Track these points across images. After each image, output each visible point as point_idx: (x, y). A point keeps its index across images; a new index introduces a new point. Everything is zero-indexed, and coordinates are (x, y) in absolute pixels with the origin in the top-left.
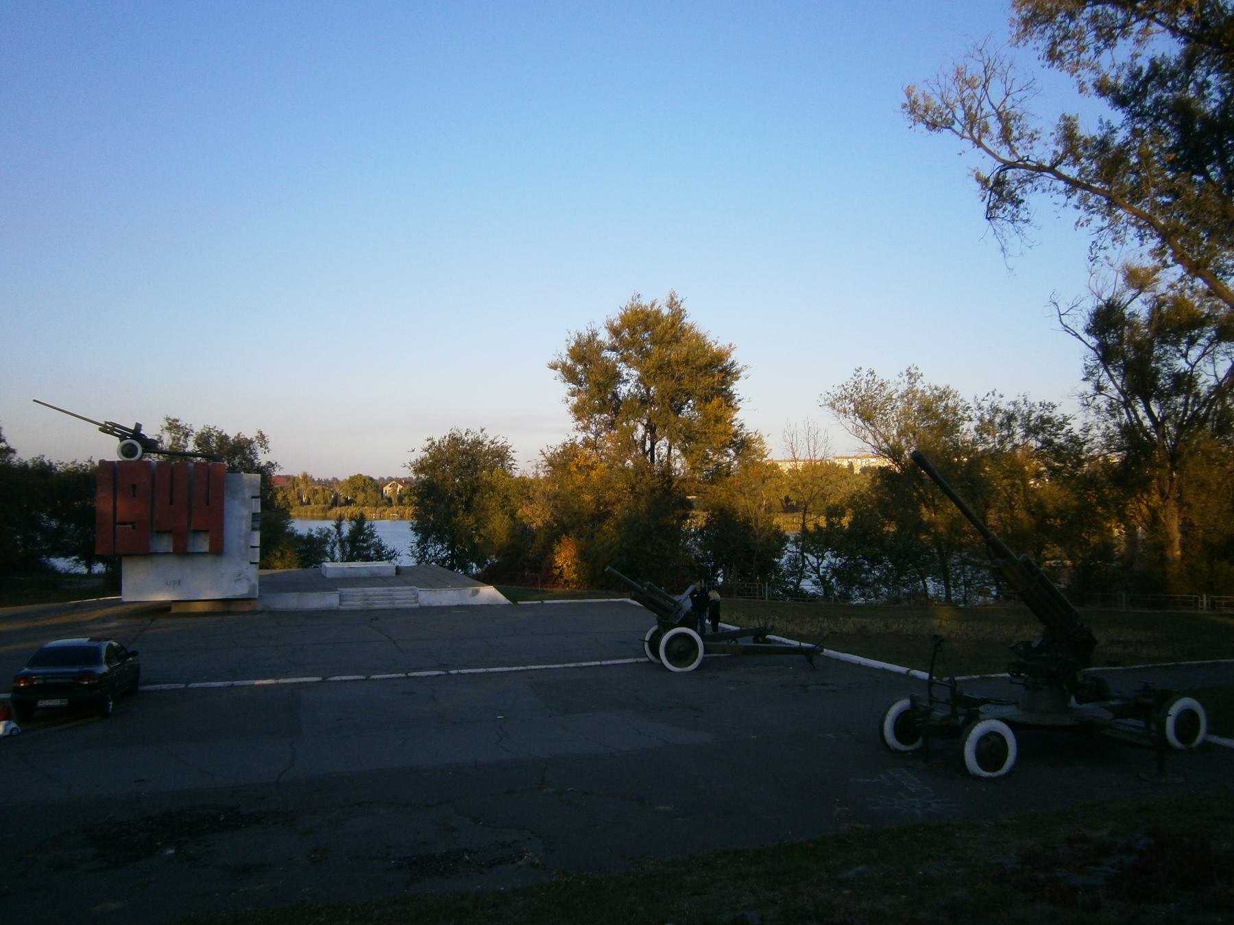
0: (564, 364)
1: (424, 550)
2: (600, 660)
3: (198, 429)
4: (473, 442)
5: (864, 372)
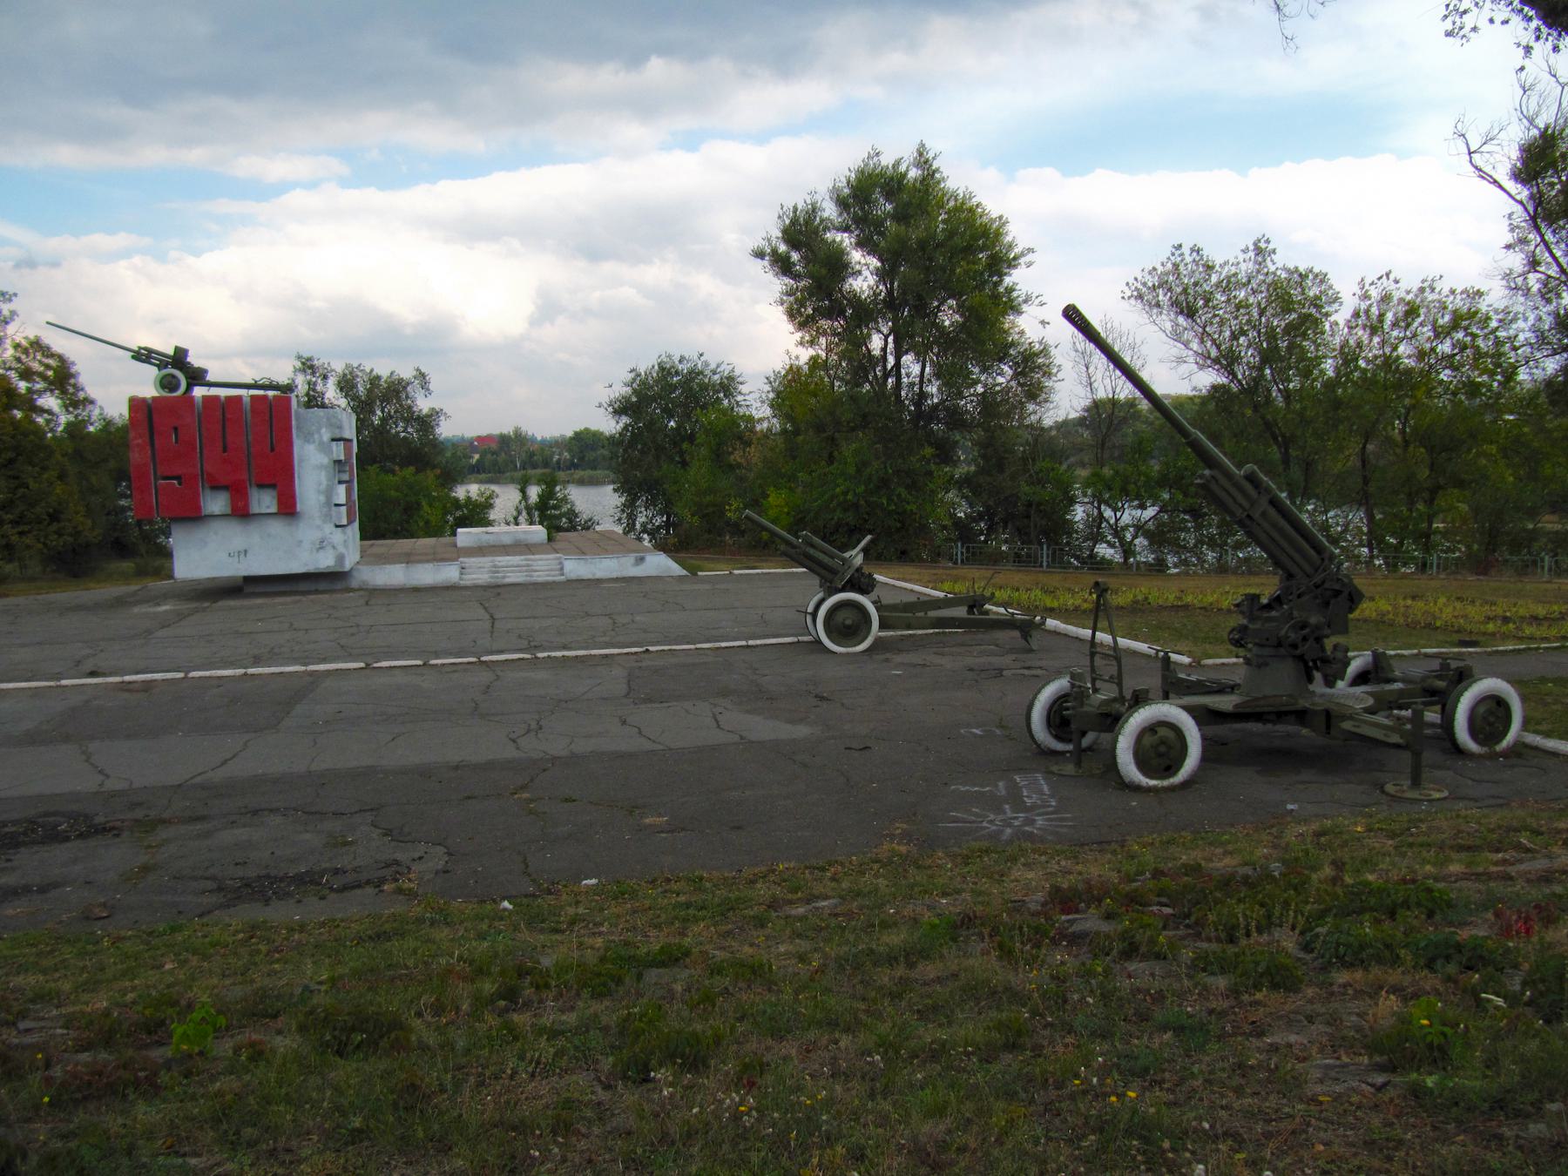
0: (774, 252)
1: (632, 518)
2: (746, 639)
3: (339, 367)
4: (691, 372)
5: (1186, 250)
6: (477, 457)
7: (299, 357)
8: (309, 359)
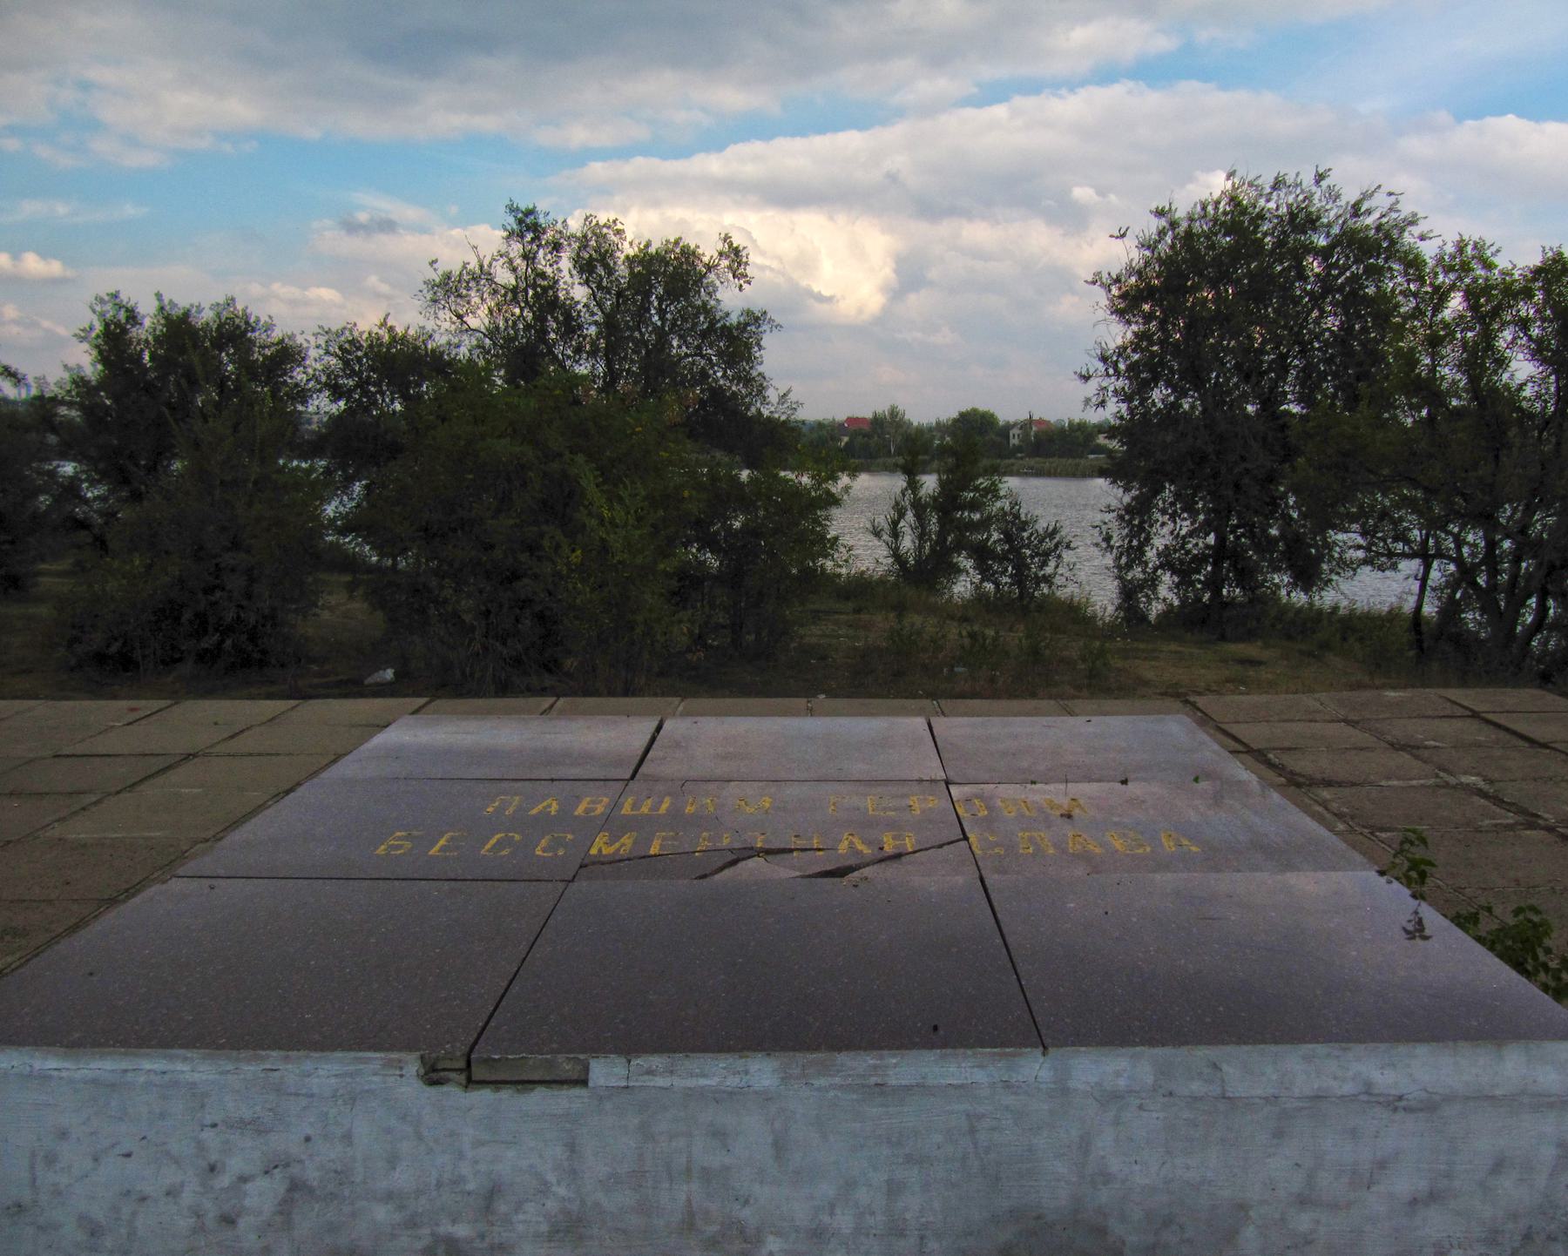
6: (846, 439)
7: (512, 209)
8: (529, 212)
